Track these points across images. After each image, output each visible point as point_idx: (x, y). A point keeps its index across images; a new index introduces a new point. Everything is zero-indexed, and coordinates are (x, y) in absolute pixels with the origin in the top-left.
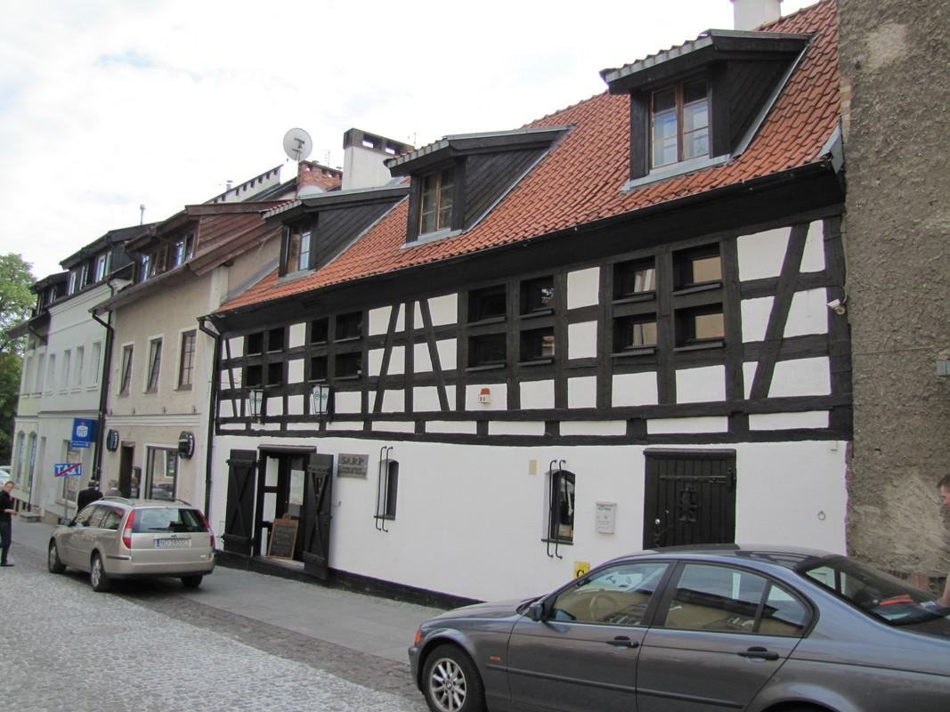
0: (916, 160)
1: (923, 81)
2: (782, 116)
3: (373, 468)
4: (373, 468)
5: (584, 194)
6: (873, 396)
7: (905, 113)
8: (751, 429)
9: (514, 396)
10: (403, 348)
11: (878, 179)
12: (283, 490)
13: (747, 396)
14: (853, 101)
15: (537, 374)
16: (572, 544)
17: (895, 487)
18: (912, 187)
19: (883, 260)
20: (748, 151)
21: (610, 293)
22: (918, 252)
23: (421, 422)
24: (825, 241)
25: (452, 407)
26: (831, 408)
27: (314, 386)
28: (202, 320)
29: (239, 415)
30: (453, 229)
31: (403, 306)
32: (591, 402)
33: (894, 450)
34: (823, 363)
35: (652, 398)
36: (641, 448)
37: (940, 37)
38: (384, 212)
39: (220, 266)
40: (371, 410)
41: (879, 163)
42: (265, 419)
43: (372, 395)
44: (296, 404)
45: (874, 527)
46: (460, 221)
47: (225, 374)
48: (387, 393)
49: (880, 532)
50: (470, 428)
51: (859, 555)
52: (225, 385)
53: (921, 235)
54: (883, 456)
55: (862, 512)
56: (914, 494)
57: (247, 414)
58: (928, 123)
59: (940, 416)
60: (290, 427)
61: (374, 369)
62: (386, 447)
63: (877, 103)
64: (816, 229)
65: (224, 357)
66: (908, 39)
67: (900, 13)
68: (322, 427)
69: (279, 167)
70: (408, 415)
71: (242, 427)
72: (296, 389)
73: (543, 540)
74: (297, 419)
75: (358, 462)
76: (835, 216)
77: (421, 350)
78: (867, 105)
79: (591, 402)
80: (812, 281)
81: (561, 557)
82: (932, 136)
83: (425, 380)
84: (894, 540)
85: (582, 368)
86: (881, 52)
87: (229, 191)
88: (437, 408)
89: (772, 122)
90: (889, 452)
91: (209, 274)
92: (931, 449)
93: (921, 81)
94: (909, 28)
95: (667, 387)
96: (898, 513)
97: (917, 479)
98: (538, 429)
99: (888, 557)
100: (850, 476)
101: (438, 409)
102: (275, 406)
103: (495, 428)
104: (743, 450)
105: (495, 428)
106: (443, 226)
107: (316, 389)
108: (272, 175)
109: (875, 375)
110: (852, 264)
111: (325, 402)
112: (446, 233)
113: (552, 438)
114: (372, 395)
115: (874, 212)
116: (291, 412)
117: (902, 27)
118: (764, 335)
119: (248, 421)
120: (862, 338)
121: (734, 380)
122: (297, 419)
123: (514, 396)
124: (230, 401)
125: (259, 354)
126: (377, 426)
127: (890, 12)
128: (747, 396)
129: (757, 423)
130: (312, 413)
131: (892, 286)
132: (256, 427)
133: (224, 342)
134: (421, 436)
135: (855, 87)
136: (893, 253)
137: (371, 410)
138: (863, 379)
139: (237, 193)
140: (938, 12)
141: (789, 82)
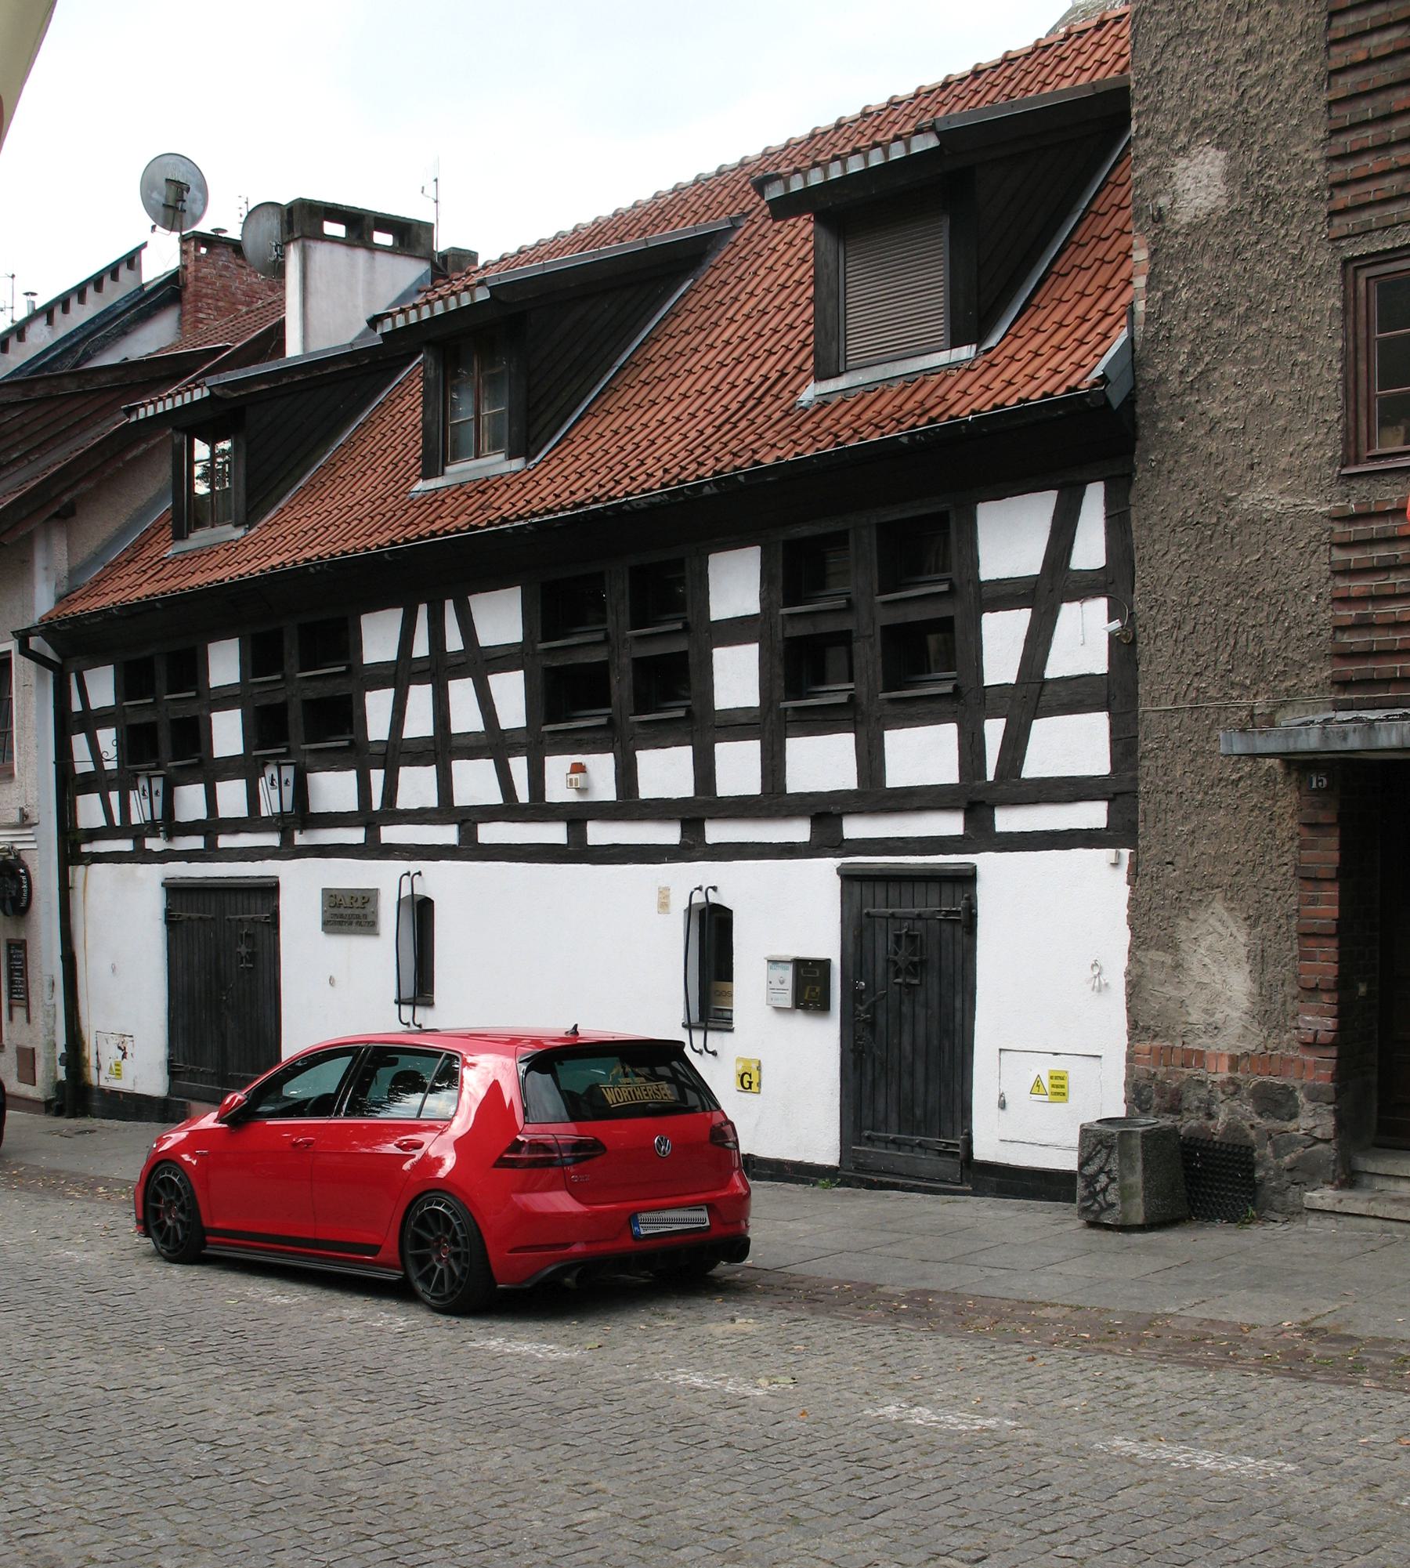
0: (1233, 392)
1: (1248, 255)
2: (1074, 266)
3: (387, 914)
4: (387, 914)
5: (717, 423)
6: (1165, 778)
7: (1223, 309)
8: (998, 829)
9: (626, 776)
10: (428, 689)
11: (1182, 420)
12: (945, 1307)
13: (990, 776)
14: (1151, 277)
15: (661, 736)
16: (731, 1031)
17: (1192, 920)
18: (1228, 437)
19: (1184, 557)
20: (1009, 338)
21: (778, 595)
22: (1232, 547)
23: (469, 824)
24: (1107, 518)
25: (523, 796)
26: (1111, 796)
27: (265, 764)
28: (23, 637)
29: (117, 823)
30: (511, 456)
31: (423, 611)
32: (752, 785)
33: (1191, 863)
34: (1099, 722)
35: (848, 780)
36: (832, 863)
37: (1272, 182)
38: (379, 392)
39: (48, 520)
40: (376, 805)
41: (1183, 394)
42: (172, 827)
43: (377, 777)
44: (232, 797)
45: (1163, 983)
46: (524, 445)
47: (79, 743)
48: (405, 773)
49: (1170, 990)
50: (555, 833)
51: (1143, 1027)
52: (83, 764)
53: (1237, 518)
54: (1177, 872)
55: (1147, 961)
56: (1215, 931)
57: (135, 819)
58: (1252, 330)
59: (1252, 811)
60: (224, 841)
61: (378, 727)
62: (408, 874)
63: (1184, 286)
64: (1094, 502)
65: (76, 706)
66: (1229, 177)
67: (1220, 129)
68: (287, 839)
69: (137, 251)
70: (445, 811)
71: (126, 845)
72: (230, 768)
73: (576, 1026)
74: (235, 826)
75: (359, 904)
76: (1123, 476)
77: (461, 691)
78: (1170, 288)
79: (752, 785)
80: (1085, 587)
81: (714, 1053)
82: (1255, 353)
83: (471, 747)
84: (1187, 1002)
85: (737, 726)
86: (1192, 195)
87: (34, 315)
88: (496, 798)
89: (1060, 275)
90: (1185, 867)
91: (29, 541)
92: (1238, 863)
93: (1244, 257)
94: (1232, 158)
95: (871, 760)
96: (1195, 961)
97: (1218, 906)
98: (669, 834)
99: (1180, 1028)
100: (1134, 904)
101: (498, 799)
102: (191, 802)
103: (599, 833)
104: (986, 863)
105: (599, 833)
106: (495, 447)
107: (271, 771)
108: (123, 272)
109: (1169, 744)
110: (1142, 559)
111: (288, 792)
112: (497, 464)
113: (692, 849)
114: (377, 777)
115: (1174, 476)
116: (223, 813)
117: (1222, 154)
118: (1016, 674)
119: (138, 834)
120: (1152, 683)
121: (971, 749)
122: (235, 826)
123: (626, 776)
124: (96, 796)
125: (151, 700)
126: (390, 834)
127: (1206, 124)
128: (990, 776)
129: (1007, 820)
130: (264, 813)
131: (1195, 600)
132: (154, 844)
133: (73, 678)
134: (470, 850)
135: (1153, 254)
136: (1197, 547)
137: (376, 805)
138: (1152, 749)
139: (50, 322)
140: (1270, 137)
141: (1105, 182)
